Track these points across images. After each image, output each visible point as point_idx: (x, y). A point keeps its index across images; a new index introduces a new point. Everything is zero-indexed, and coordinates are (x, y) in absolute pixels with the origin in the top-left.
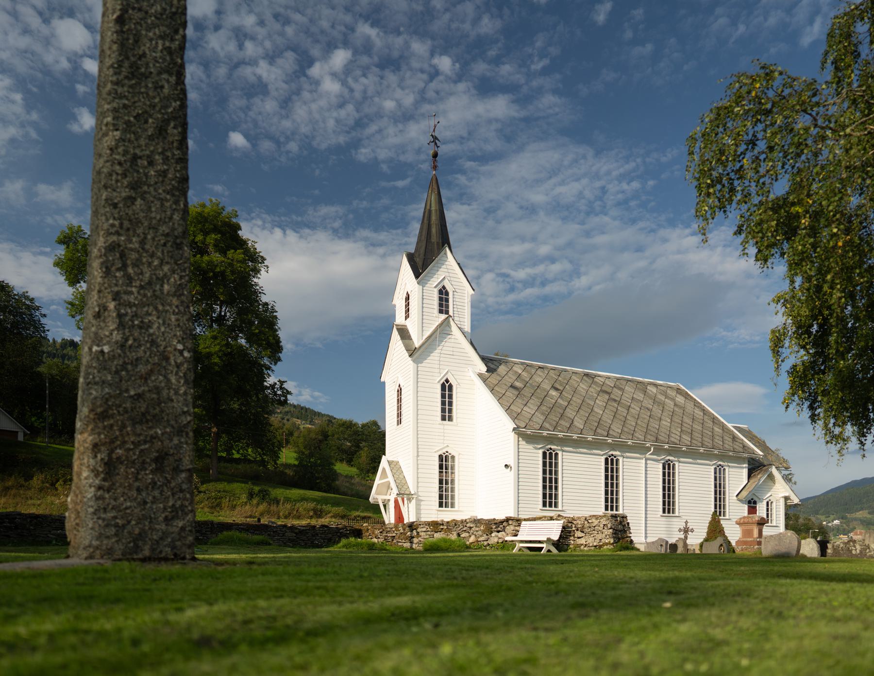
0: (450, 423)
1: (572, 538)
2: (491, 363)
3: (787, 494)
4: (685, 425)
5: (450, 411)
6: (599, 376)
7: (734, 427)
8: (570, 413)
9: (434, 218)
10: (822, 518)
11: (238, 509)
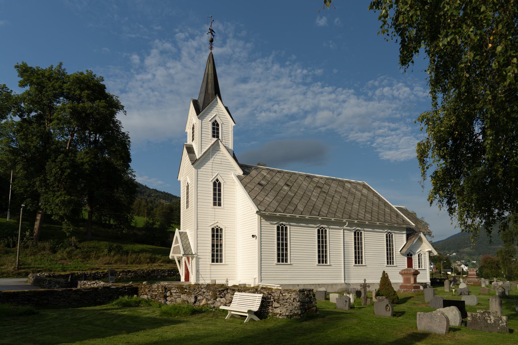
0: (219, 207)
1: (270, 308)
2: (245, 168)
3: (430, 250)
4: (367, 207)
5: (220, 200)
6: (316, 177)
7: (397, 208)
8: (295, 201)
9: (211, 77)
10: (447, 252)
11: (101, 259)
